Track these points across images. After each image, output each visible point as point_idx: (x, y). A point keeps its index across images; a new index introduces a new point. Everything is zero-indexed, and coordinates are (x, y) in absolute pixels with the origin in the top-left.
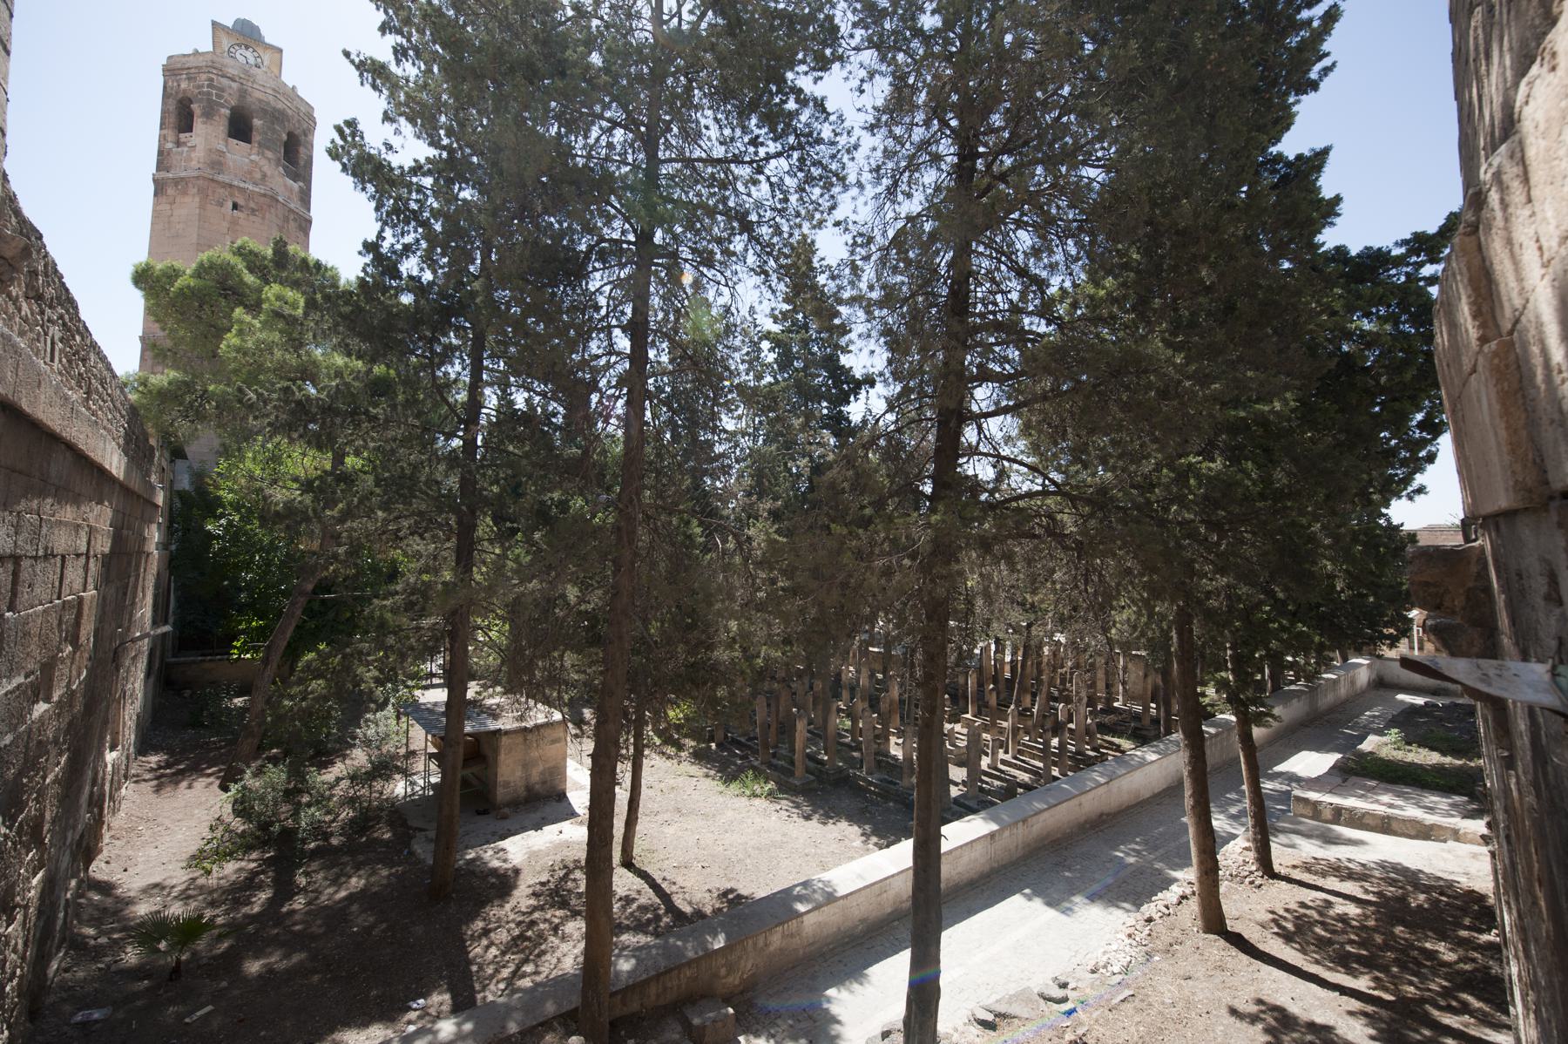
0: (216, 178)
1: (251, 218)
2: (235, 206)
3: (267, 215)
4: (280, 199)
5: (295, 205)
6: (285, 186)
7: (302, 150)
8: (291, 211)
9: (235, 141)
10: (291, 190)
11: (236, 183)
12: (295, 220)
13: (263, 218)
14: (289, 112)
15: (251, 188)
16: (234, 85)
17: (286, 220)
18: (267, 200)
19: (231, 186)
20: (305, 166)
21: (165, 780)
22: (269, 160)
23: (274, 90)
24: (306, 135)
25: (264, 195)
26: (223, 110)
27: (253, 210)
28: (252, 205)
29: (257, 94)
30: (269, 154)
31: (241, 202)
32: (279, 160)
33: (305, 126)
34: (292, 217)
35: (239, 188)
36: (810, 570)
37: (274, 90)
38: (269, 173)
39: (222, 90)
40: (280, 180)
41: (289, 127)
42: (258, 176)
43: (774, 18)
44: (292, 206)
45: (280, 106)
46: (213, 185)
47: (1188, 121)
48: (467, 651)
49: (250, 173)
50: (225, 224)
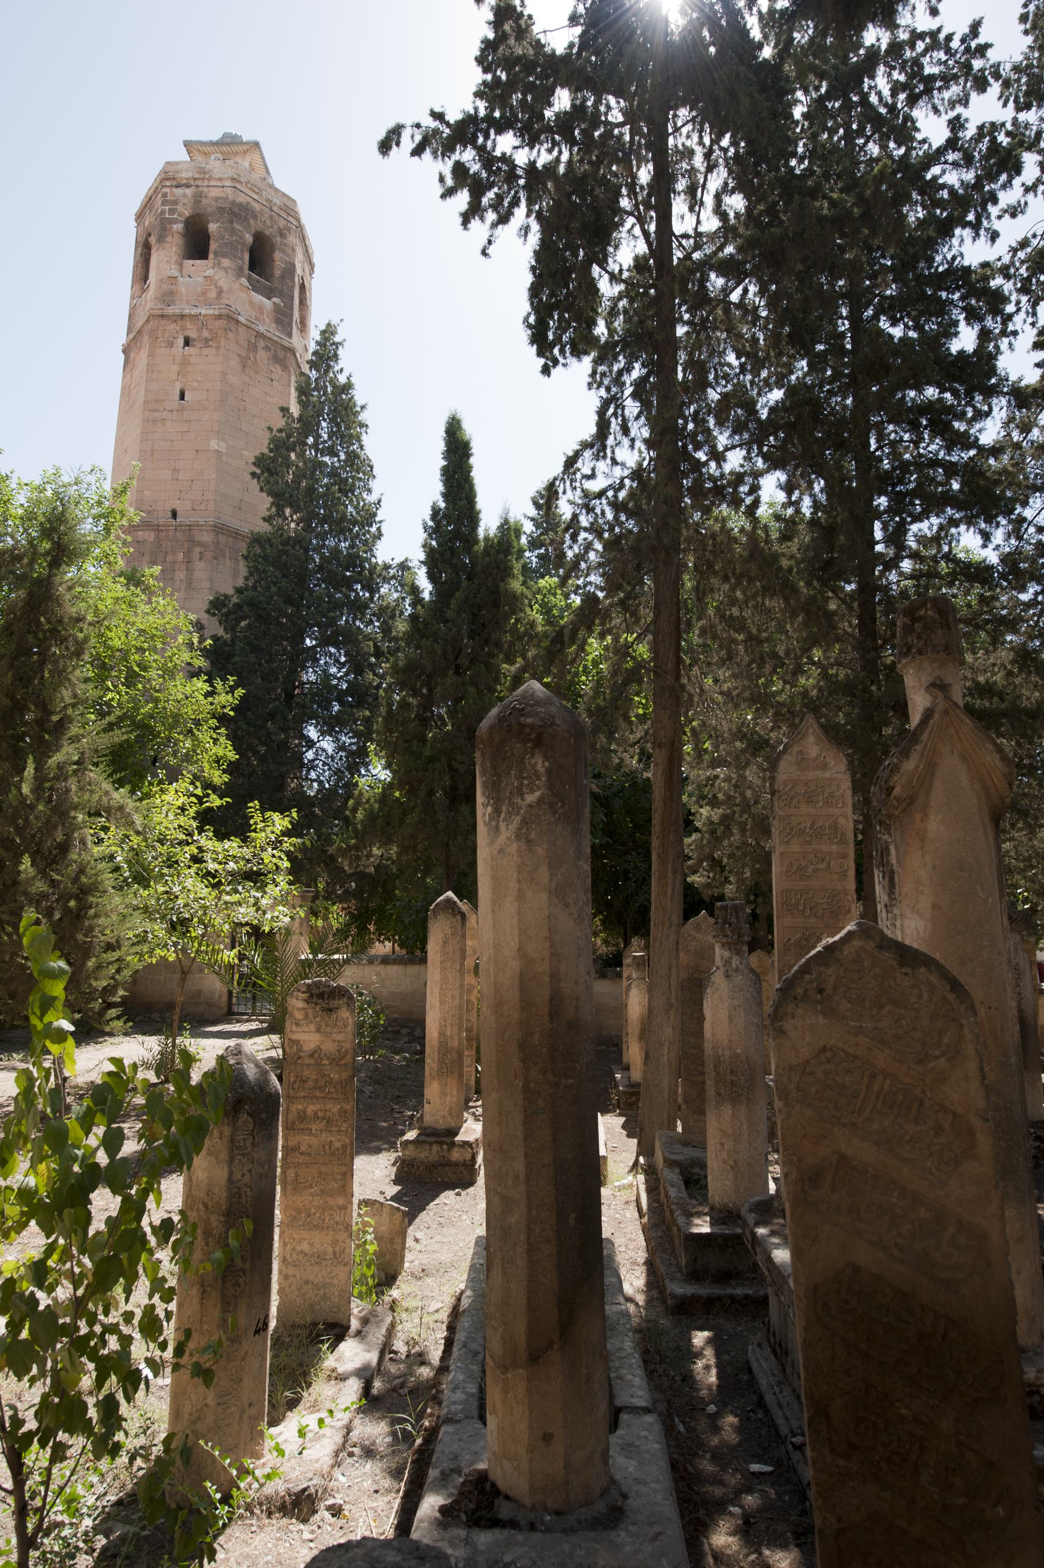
0: (165, 312)
1: (205, 351)
2: (187, 342)
3: (223, 342)
4: (241, 319)
5: (267, 326)
6: (251, 302)
7: (278, 255)
8: (259, 335)
9: (191, 262)
10: (261, 309)
11: (187, 312)
12: (267, 348)
13: (218, 348)
14: (257, 207)
15: (203, 312)
16: (189, 192)
17: (253, 347)
18: (223, 323)
19: (182, 317)
20: (282, 277)
21: (873, 45)
22: (226, 270)
23: (233, 179)
24: (282, 235)
25: (220, 317)
26: (175, 227)
27: (207, 340)
28: (206, 334)
29: (215, 193)
30: (226, 262)
31: (193, 334)
32: (240, 269)
33: (282, 223)
34: (261, 344)
35: (191, 316)
36: (62, 513)
37: (233, 179)
38: (225, 287)
39: (175, 202)
40: (243, 296)
41: (256, 225)
42: (213, 295)
43: (702, 433)
44: (262, 329)
45: (242, 199)
46: (163, 322)
47: (735, 612)
48: (719, 1376)
49: (204, 293)
50: (175, 368)
